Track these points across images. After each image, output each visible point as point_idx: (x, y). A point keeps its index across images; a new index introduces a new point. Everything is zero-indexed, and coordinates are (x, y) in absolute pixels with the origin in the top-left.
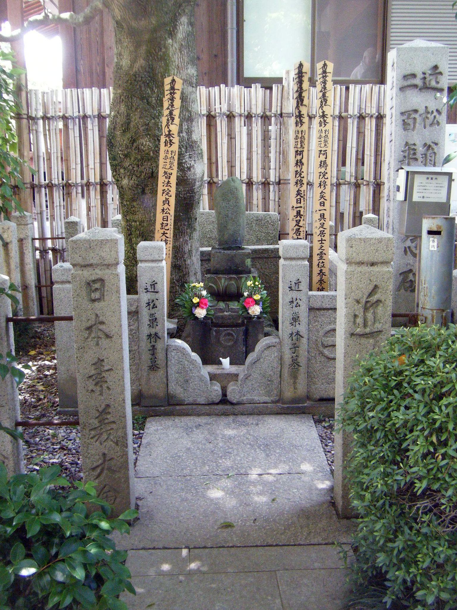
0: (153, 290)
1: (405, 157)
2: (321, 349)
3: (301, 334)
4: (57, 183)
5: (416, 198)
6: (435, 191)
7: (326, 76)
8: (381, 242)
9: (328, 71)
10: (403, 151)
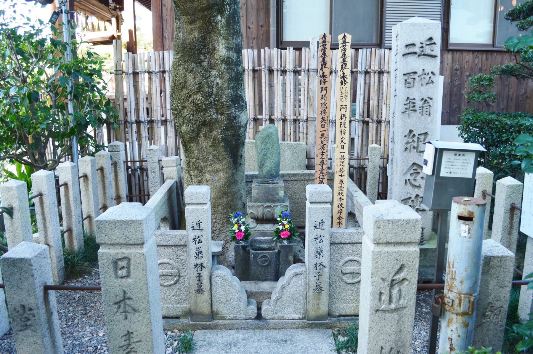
0: (198, 228)
1: (406, 109)
2: (341, 275)
3: (324, 264)
4: (143, 120)
5: (443, 173)
6: (462, 167)
7: (345, 46)
8: (409, 223)
9: (347, 41)
10: (405, 105)
